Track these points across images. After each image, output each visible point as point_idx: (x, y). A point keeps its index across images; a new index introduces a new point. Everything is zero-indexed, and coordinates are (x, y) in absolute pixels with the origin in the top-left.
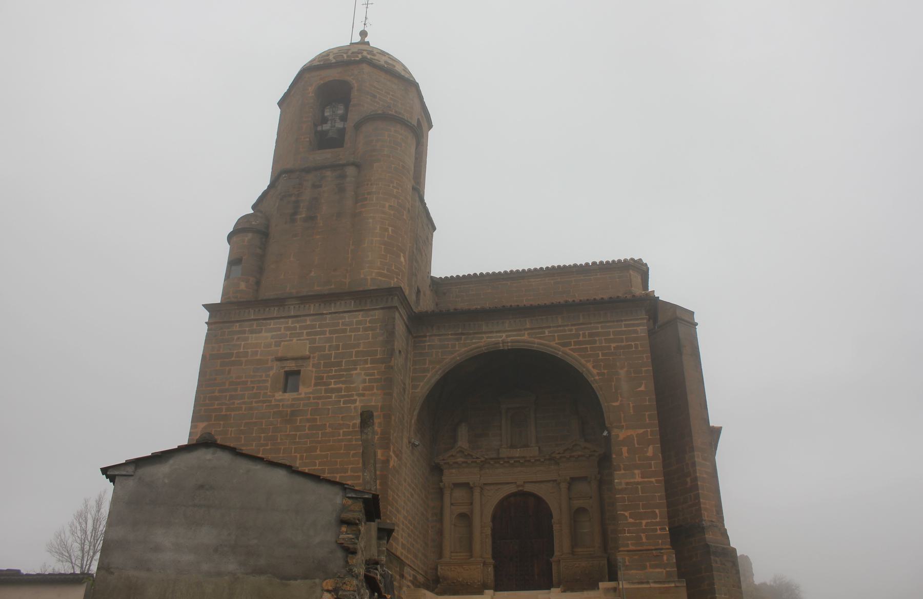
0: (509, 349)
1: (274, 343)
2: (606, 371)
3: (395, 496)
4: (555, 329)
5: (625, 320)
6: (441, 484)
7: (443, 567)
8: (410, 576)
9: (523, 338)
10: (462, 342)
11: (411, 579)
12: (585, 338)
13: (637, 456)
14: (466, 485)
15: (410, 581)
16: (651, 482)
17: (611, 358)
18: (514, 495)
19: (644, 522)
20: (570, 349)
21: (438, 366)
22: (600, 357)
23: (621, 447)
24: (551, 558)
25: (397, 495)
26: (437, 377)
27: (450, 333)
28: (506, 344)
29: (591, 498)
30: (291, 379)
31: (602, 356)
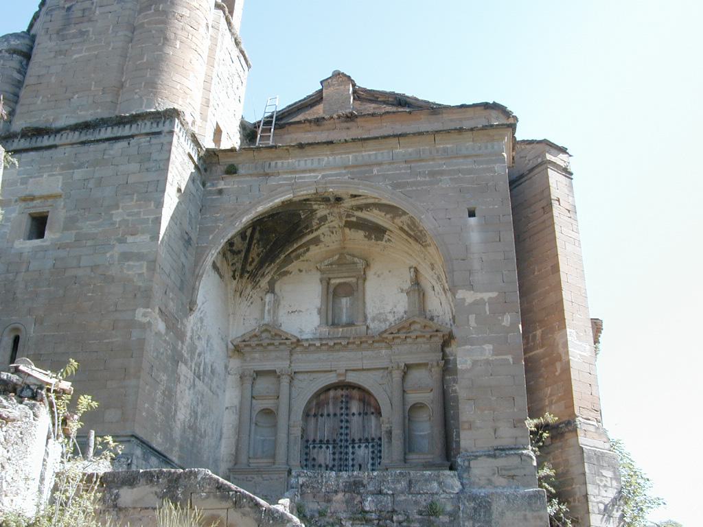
1: (19, 181)
7: (236, 476)
30: (39, 225)
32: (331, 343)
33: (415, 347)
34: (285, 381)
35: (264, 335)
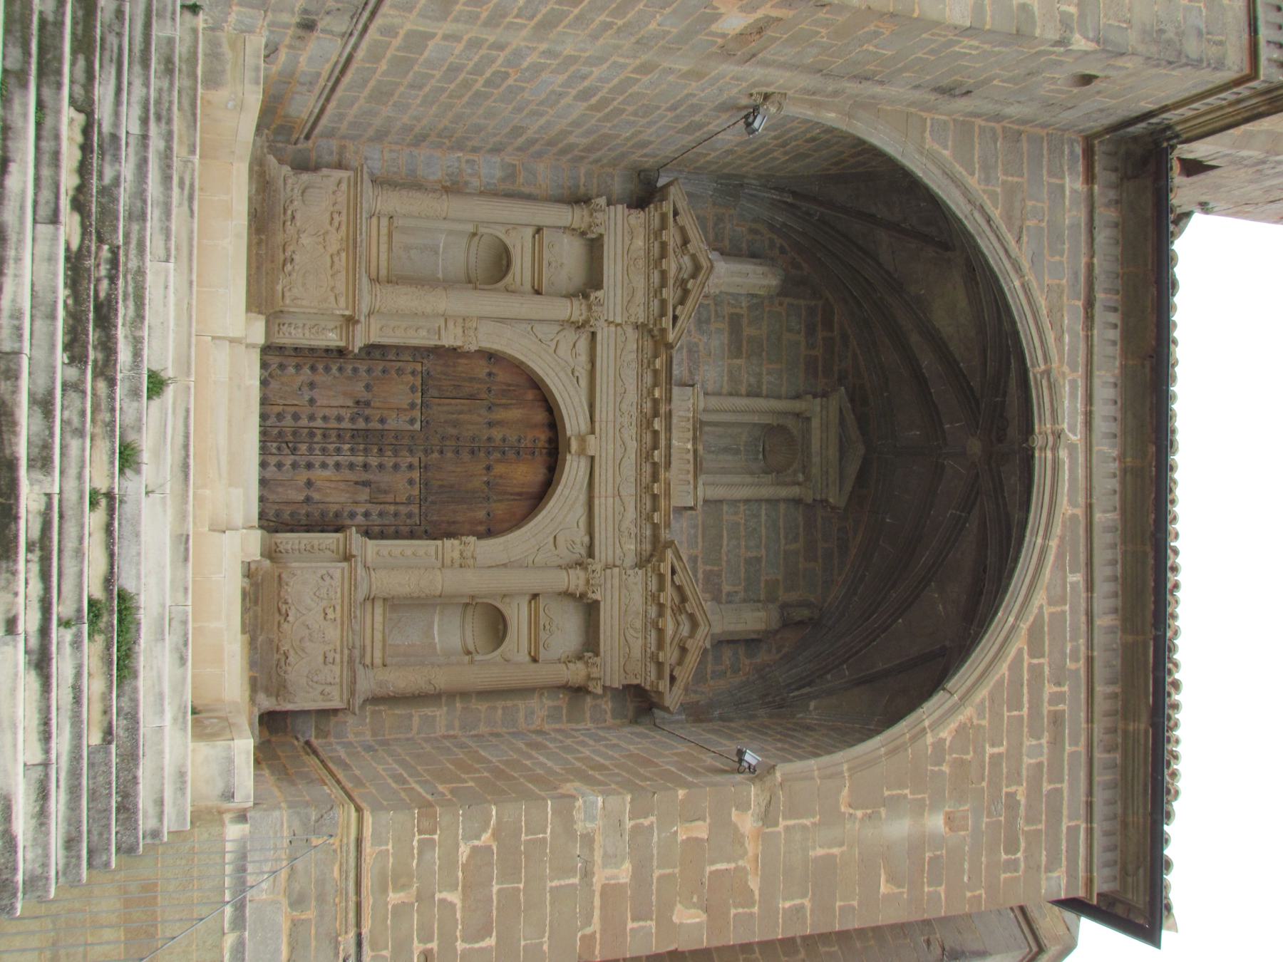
5: (1090, 832)
7: (344, 186)
12: (1050, 703)
14: (593, 280)
16: (588, 921)
17: (984, 784)
19: (455, 898)
20: (1020, 651)
22: (989, 750)
23: (708, 820)
24: (357, 532)
25: (607, 26)
29: (535, 660)
31: (992, 756)
32: (657, 425)
33: (638, 624)
34: (575, 310)
35: (686, 260)
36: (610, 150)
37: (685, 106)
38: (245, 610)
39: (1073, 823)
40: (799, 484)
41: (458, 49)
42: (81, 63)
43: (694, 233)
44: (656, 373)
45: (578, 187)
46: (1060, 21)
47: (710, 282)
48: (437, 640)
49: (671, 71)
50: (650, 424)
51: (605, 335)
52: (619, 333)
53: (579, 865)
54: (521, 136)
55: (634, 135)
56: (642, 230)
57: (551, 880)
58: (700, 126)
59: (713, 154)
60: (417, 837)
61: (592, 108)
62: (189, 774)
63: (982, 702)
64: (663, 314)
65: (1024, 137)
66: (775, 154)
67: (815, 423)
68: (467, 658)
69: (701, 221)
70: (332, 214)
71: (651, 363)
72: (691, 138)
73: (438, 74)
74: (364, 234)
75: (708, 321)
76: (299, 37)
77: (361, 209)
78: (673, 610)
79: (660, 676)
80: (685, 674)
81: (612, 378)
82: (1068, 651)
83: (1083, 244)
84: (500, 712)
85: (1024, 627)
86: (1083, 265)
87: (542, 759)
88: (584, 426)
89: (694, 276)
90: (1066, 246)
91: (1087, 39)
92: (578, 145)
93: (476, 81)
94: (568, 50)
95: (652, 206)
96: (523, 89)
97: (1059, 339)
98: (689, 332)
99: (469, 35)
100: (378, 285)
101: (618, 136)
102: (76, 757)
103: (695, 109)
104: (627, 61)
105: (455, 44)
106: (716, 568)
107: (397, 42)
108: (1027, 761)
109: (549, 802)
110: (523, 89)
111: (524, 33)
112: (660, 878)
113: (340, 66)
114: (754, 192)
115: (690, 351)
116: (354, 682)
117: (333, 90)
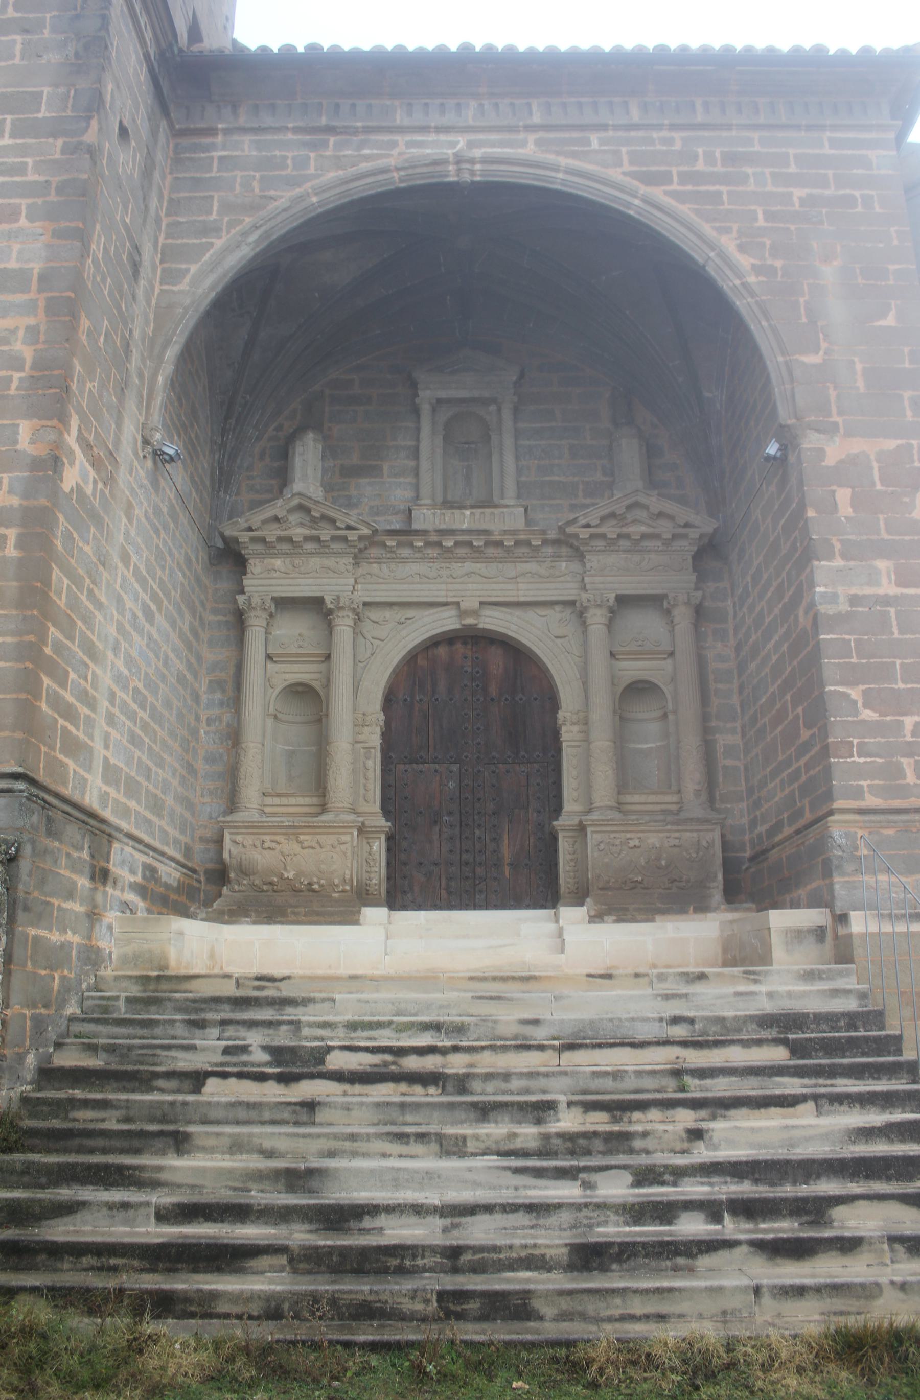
0: (473, 182)
2: (778, 264)
3: (84, 598)
4: (620, 134)
6: (241, 599)
7: (239, 838)
8: (133, 872)
9: (520, 151)
10: (328, 153)
11: (139, 878)
13: (881, 517)
15: (135, 887)
17: (792, 227)
18: (449, 639)
20: (666, 193)
21: (247, 220)
22: (761, 222)
23: (834, 488)
24: (557, 819)
25: (91, 594)
26: (245, 252)
27: (290, 125)
28: (468, 166)
36: (193, 593)
37: (155, 521)
38: (634, 920)
39: (827, 144)
40: (499, 410)
41: (114, 734)
42: (161, 1083)
43: (269, 513)
44: (399, 544)
45: (227, 621)
46: (71, 154)
47: (314, 496)
48: (653, 745)
49: (127, 533)
50: (449, 550)
51: (363, 595)
52: (363, 581)
53: (878, 608)
54: (185, 676)
55: (181, 570)
56: (266, 561)
57: (893, 633)
58: (172, 508)
59: (194, 494)
60: (856, 759)
61: (160, 609)
62: (805, 967)
63: (717, 229)
64: (345, 539)
65: (174, 196)
66: (193, 436)
67: (442, 394)
68: (671, 717)
69: (256, 505)
70: (264, 849)
71: (390, 550)
72: (181, 515)
73: (137, 754)
74: (282, 819)
75: (349, 498)
76: (115, 883)
77: (259, 822)
78: (623, 526)
79: (684, 536)
80: (683, 514)
81: (405, 586)
82: (665, 148)
83: (276, 137)
84: (720, 686)
85: (643, 189)
86: (295, 137)
87: (770, 645)
88: (451, 612)
89: (308, 511)
90: (277, 153)
91: (87, 128)
92: (191, 623)
93: (141, 718)
94: (112, 630)
95: (243, 552)
96: (146, 674)
97: (367, 158)
98: (359, 515)
99: (104, 724)
100: (329, 806)
101: (182, 584)
102: (799, 1072)
103: (157, 512)
104: (119, 575)
105: (112, 738)
106: (581, 487)
107: (112, 791)
108: (769, 188)
109: (822, 637)
110: (146, 674)
111: (99, 671)
112: (889, 532)
113: (137, 845)
114: (226, 456)
115: (377, 514)
116: (699, 821)
117: (154, 850)
